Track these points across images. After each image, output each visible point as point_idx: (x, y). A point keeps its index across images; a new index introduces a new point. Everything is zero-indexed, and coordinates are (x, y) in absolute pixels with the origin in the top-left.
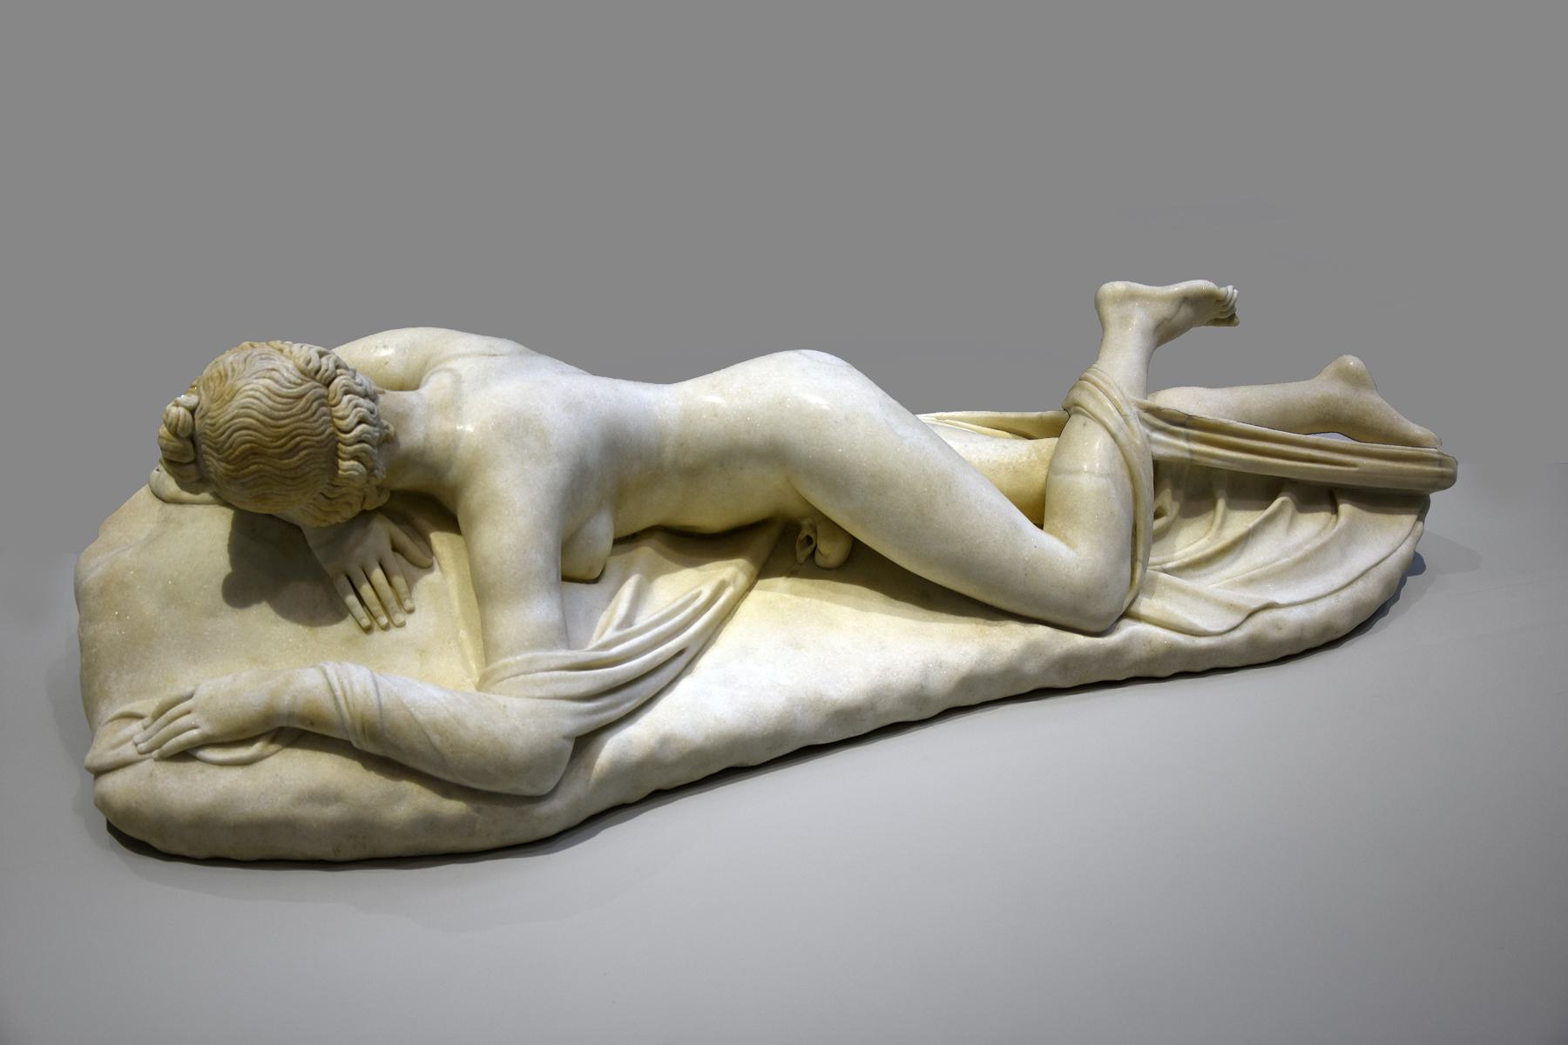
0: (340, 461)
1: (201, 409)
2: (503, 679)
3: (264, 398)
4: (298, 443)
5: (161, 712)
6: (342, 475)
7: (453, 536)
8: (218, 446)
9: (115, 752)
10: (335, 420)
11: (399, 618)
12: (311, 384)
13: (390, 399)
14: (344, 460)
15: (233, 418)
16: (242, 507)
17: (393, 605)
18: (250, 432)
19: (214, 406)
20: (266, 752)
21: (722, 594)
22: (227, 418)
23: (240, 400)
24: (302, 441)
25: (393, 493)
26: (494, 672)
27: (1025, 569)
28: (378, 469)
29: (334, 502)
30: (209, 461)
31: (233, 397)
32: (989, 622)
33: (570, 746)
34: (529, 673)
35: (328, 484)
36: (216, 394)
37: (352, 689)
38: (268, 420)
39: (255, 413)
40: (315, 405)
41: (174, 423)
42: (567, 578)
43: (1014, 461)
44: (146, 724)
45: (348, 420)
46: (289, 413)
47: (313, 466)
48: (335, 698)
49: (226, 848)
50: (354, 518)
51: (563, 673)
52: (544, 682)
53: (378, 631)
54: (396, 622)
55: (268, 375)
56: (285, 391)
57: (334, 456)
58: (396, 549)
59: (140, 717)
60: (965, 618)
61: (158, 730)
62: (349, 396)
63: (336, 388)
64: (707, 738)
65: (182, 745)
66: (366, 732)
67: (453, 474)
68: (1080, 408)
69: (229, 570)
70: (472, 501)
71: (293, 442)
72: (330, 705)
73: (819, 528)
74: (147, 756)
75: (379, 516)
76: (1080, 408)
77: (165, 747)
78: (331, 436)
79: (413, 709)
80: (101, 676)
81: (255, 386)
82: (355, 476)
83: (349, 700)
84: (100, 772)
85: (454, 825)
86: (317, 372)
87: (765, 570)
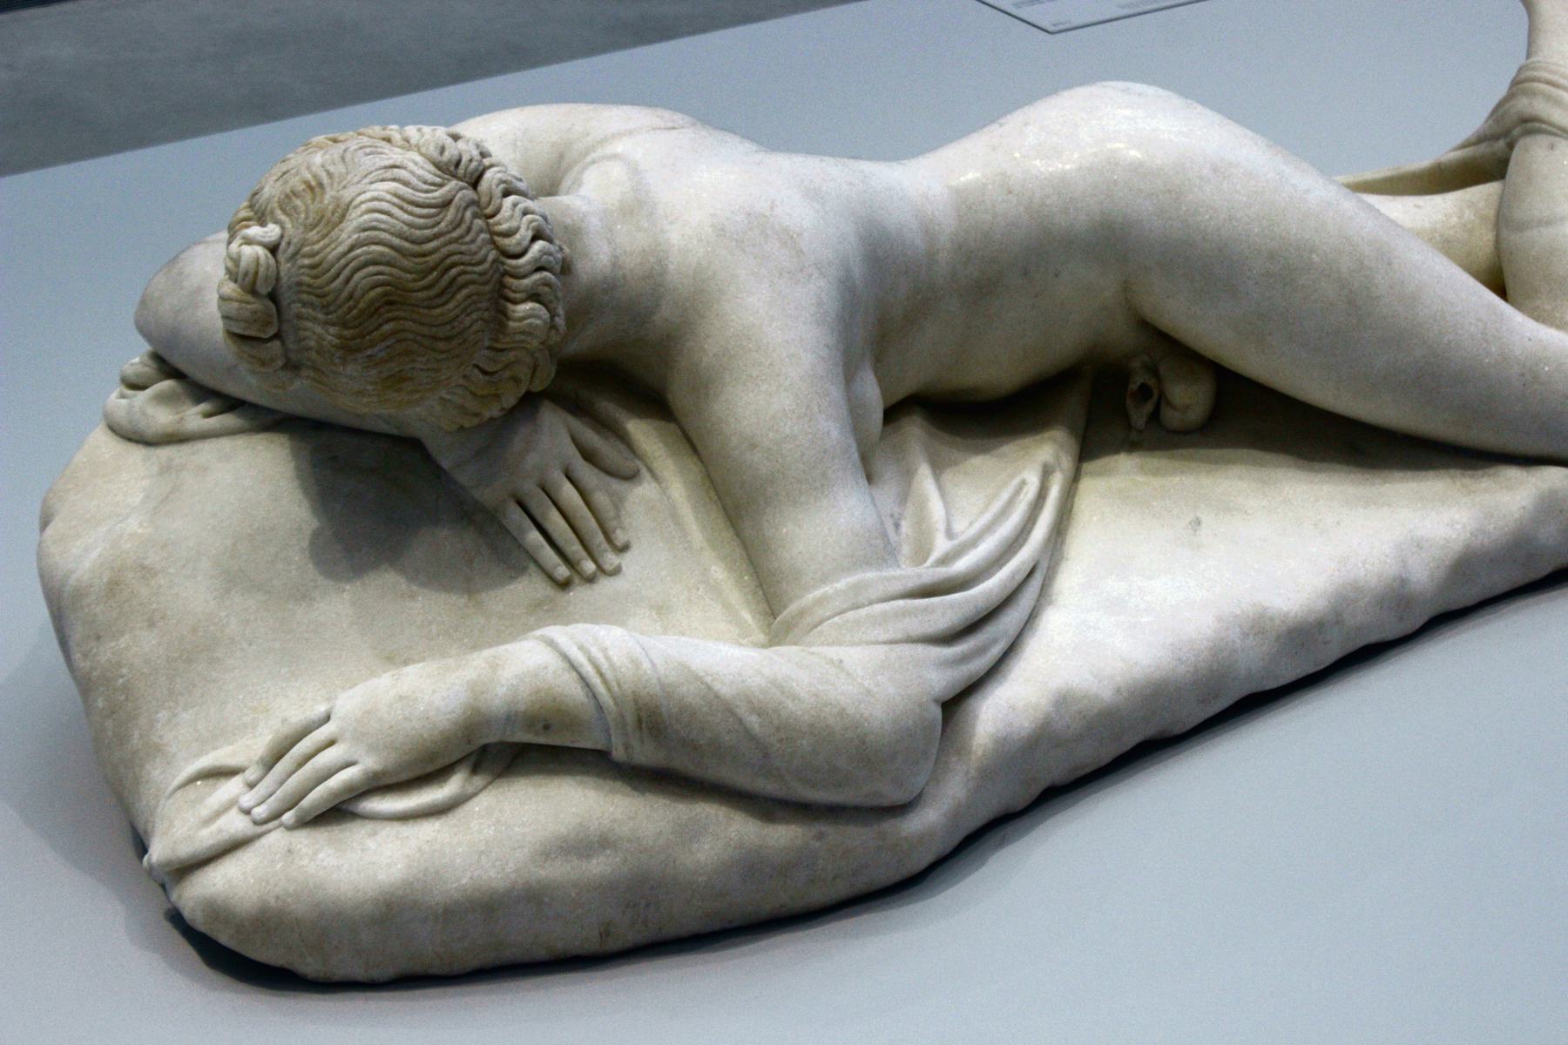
0: (510, 306)
1: (289, 244)
2: (821, 622)
3: (395, 211)
4: (454, 279)
5: (277, 755)
9: (214, 827)
10: (496, 238)
11: (611, 559)
12: (453, 184)
14: (515, 302)
15: (352, 248)
18: (381, 268)
19: (313, 235)
20: (470, 789)
22: (341, 249)
23: (356, 219)
24: (460, 274)
27: (1523, 375)
30: (306, 329)
31: (343, 216)
33: (937, 712)
34: (863, 606)
35: (490, 348)
36: (312, 216)
37: (608, 658)
38: (407, 245)
41: (252, 271)
43: (1438, 226)
45: (518, 236)
46: (436, 230)
47: (474, 316)
48: (583, 679)
49: (428, 949)
51: (901, 602)
52: (884, 618)
53: (578, 585)
54: (608, 567)
56: (420, 197)
57: (500, 296)
58: (589, 456)
60: (1431, 473)
61: (282, 783)
62: (512, 198)
63: (490, 188)
65: (335, 794)
66: (644, 725)
67: (666, 313)
68: (1537, 125)
69: (315, 523)
71: (446, 278)
73: (1163, 369)
74: (270, 825)
76: (1537, 125)
77: (306, 803)
78: (495, 266)
79: (708, 679)
80: (143, 721)
81: (375, 194)
82: (537, 326)
83: (609, 675)
85: (785, 868)
86: (458, 164)
87: (1089, 449)
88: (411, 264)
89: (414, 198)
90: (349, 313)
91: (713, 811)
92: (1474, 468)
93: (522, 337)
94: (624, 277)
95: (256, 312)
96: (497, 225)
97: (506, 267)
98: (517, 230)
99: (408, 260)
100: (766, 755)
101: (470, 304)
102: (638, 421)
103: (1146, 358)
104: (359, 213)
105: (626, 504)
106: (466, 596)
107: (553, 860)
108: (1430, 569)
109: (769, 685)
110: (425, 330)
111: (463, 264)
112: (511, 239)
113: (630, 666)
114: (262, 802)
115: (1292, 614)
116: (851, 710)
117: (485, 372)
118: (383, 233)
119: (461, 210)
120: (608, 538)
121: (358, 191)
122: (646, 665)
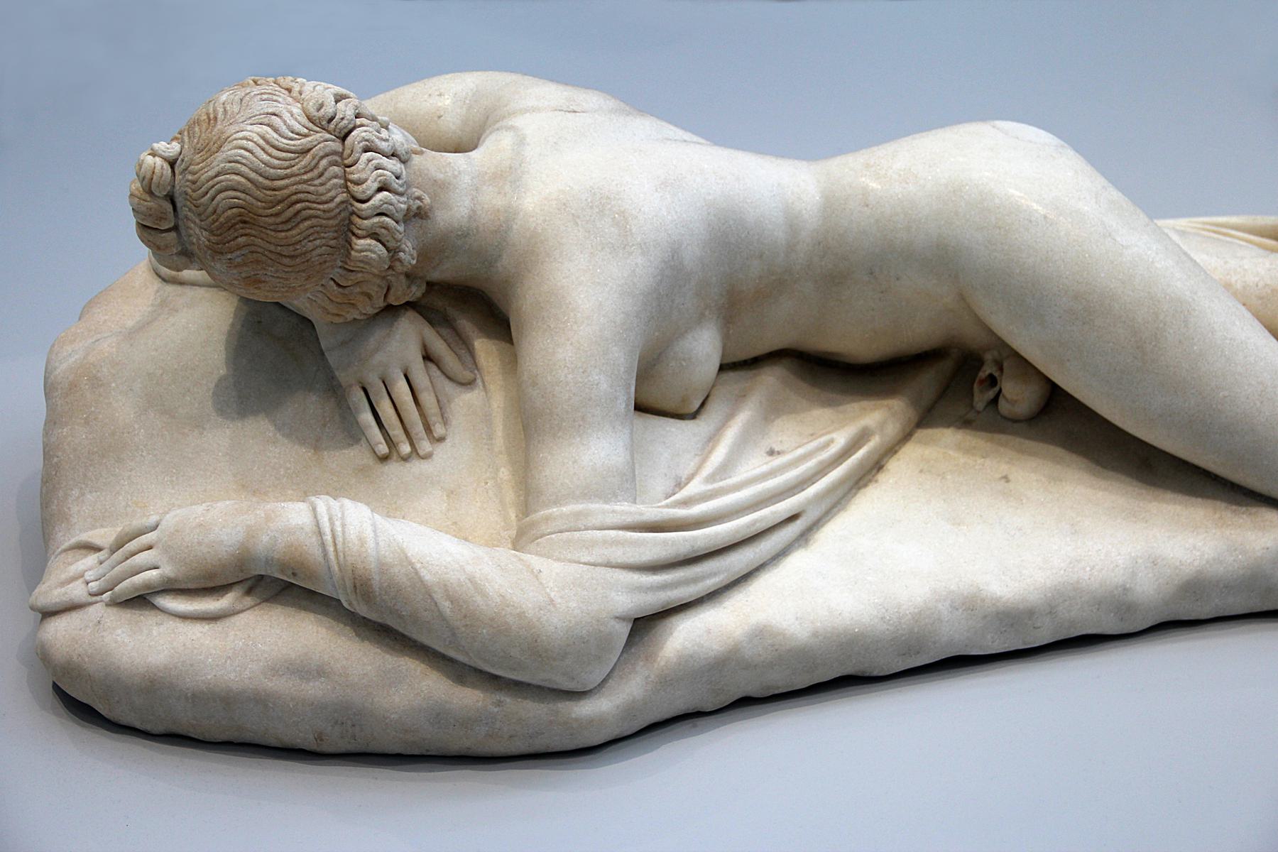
0: (353, 238)
1: (183, 160)
4: (299, 212)
6: (356, 257)
7: (508, 345)
8: (201, 209)
10: (349, 184)
13: (433, 163)
14: (359, 237)
16: (242, 295)
17: (418, 428)
18: (239, 194)
19: (197, 158)
20: (239, 607)
21: (863, 445)
22: (210, 173)
23: (228, 152)
25: (430, 285)
26: (533, 525)
28: (404, 252)
29: (346, 291)
32: (1234, 507)
33: (624, 630)
34: (579, 530)
39: (243, 169)
40: (324, 162)
41: (148, 176)
42: (641, 408)
44: (102, 558)
45: (364, 186)
47: (318, 242)
48: (323, 545)
49: (185, 720)
50: (377, 314)
51: (621, 533)
53: (397, 461)
54: (421, 453)
55: (266, 121)
56: (283, 142)
57: (346, 229)
59: (97, 549)
64: (815, 634)
66: (358, 591)
67: (506, 262)
70: (524, 304)
72: (316, 552)
73: (1005, 364)
74: (98, 598)
75: (411, 314)
79: (418, 566)
80: (61, 494)
83: (340, 546)
84: (48, 614)
87: (927, 417)
88: (262, 195)
89: (277, 142)
90: (213, 224)
91: (413, 667)
92: (1239, 504)
93: (362, 265)
94: (477, 228)
95: (151, 209)
96: (351, 173)
97: (353, 208)
98: (366, 180)
99: (260, 191)
100: (454, 634)
101: (312, 234)
102: (485, 340)
103: (996, 353)
104: (230, 147)
105: (452, 405)
106: (313, 451)
107: (281, 676)
108: (1159, 584)
109: (467, 581)
110: (272, 248)
111: (308, 201)
112: (359, 187)
113: (357, 543)
114: (97, 580)
115: (1004, 599)
116: (530, 614)
117: (338, 285)
118: (244, 167)
119: (317, 158)
120: (428, 429)
121: (237, 129)
122: (371, 544)
